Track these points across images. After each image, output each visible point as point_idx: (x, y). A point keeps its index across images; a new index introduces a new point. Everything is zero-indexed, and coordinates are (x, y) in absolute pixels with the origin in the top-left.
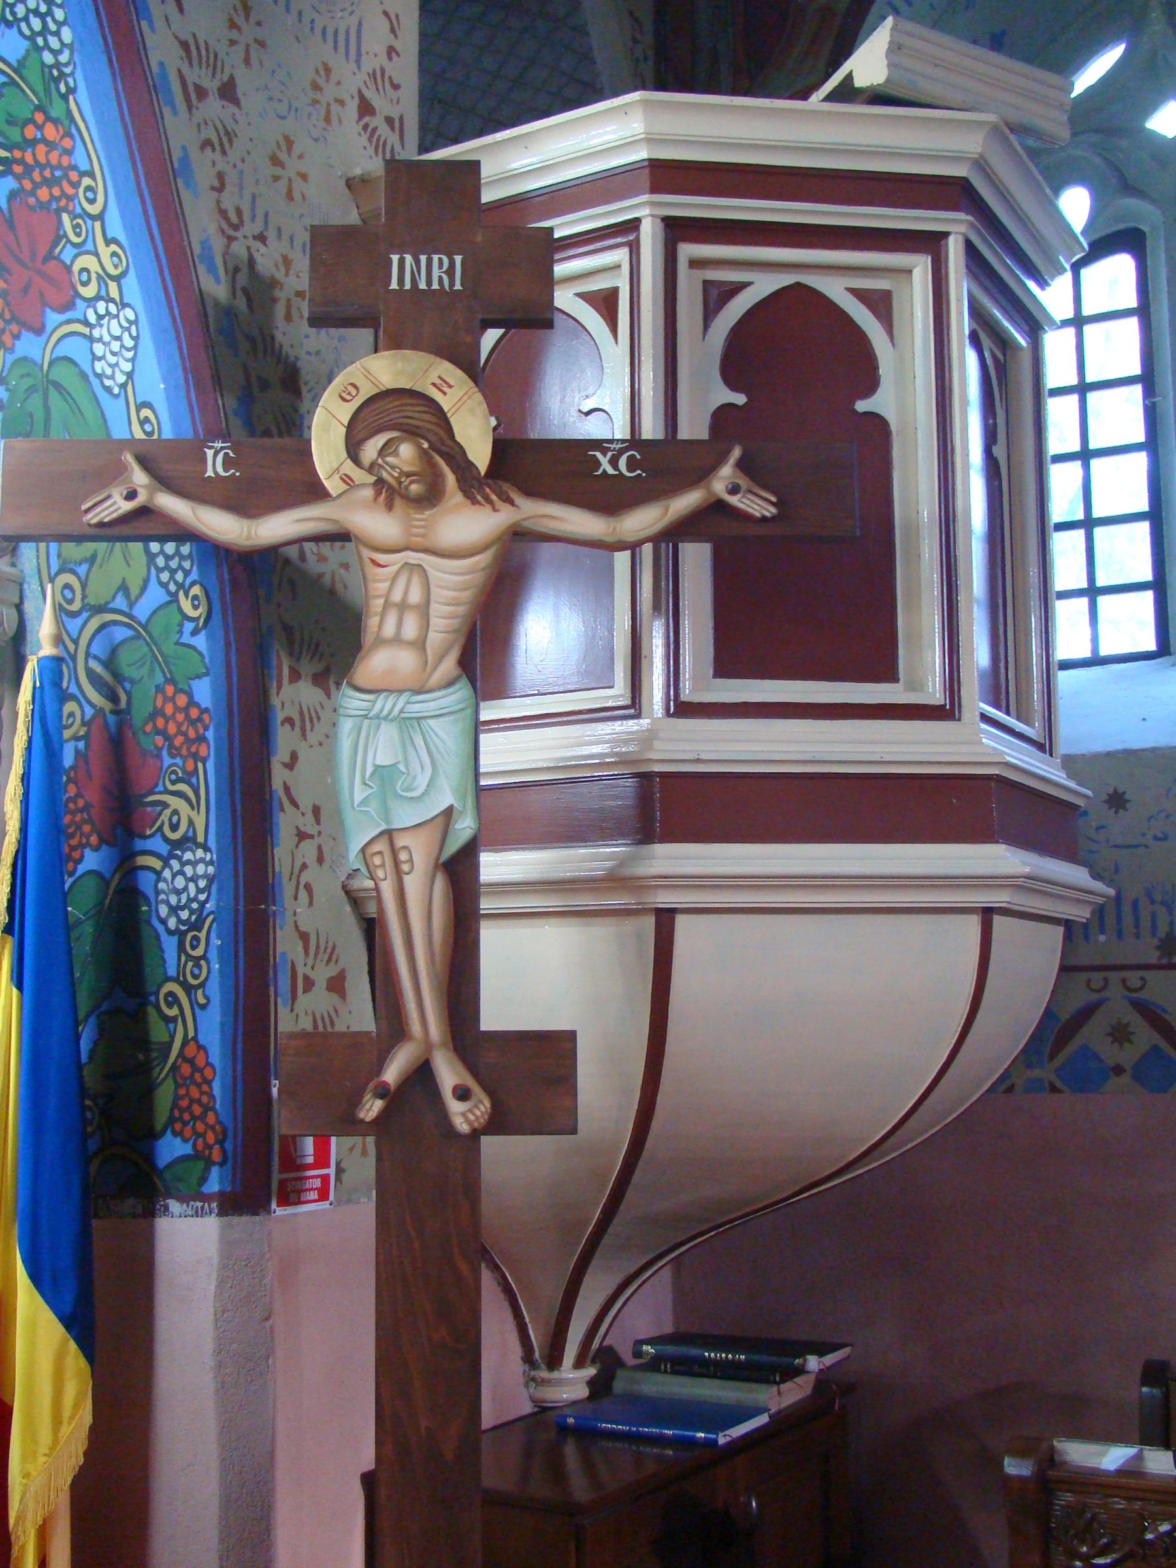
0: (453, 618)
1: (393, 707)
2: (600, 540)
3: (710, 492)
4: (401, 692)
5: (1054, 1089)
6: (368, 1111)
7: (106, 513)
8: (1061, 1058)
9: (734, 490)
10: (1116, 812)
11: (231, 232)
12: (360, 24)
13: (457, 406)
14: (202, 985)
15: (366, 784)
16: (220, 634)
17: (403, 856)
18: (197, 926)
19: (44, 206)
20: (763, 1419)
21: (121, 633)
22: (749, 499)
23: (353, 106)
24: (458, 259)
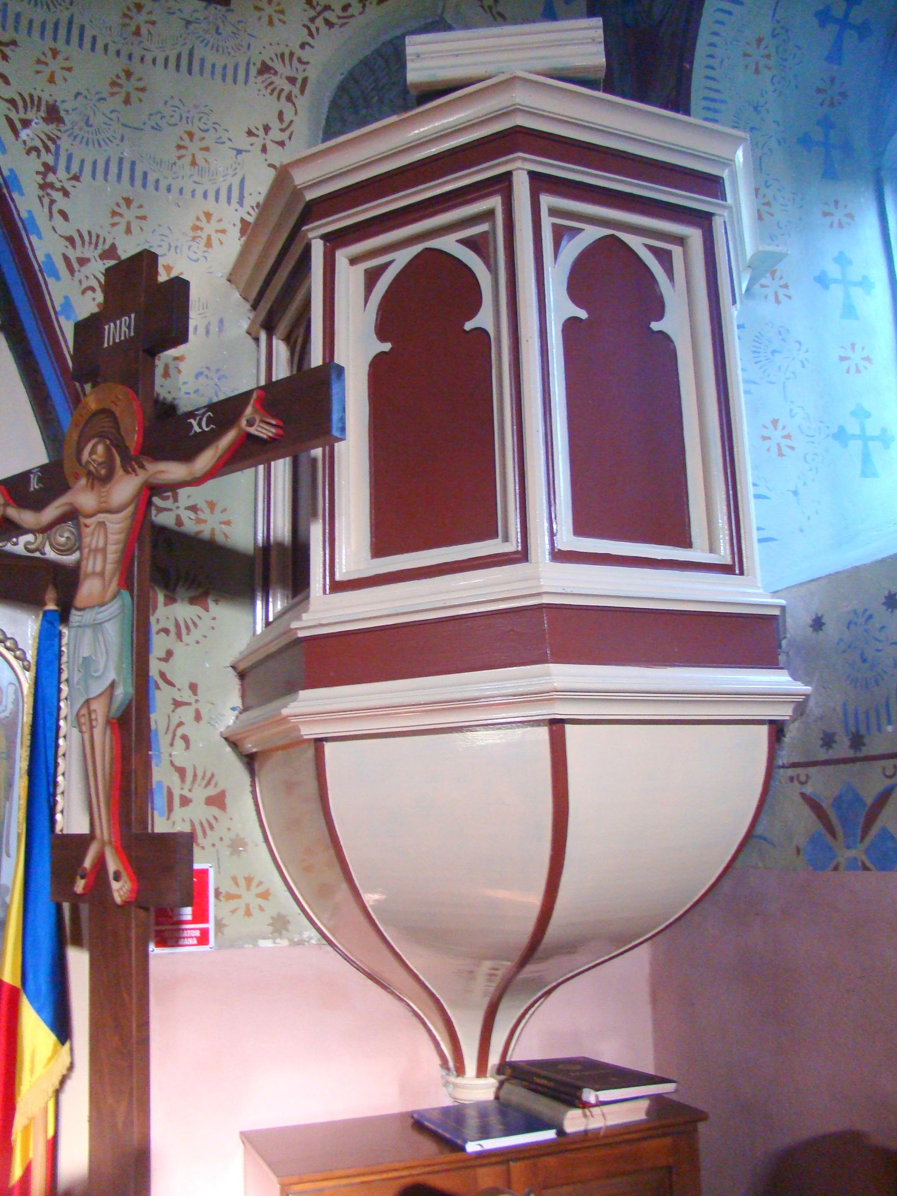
5: (865, 868)
8: (868, 839)
10: (892, 612)
12: (242, 181)
17: (93, 716)
24: (133, 316)
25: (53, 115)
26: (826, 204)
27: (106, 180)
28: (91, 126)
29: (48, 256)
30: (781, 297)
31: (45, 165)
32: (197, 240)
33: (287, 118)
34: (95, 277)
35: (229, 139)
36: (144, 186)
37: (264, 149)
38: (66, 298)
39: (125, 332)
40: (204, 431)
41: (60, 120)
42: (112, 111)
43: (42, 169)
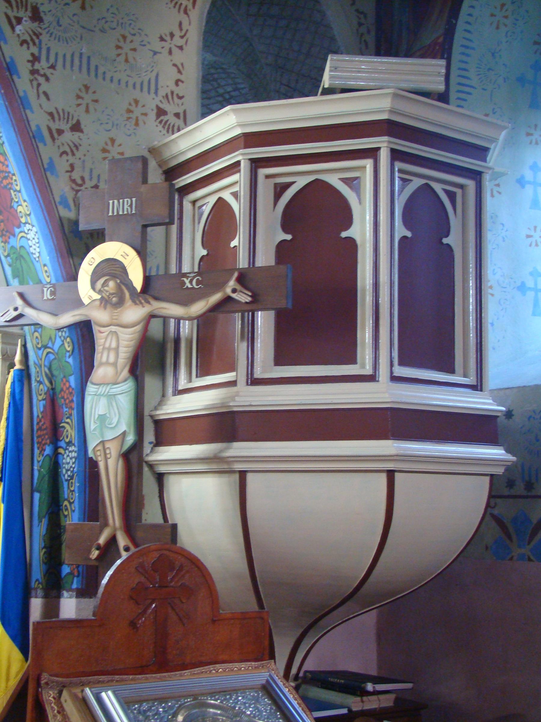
0: (127, 353)
1: (102, 390)
2: (182, 317)
3: (225, 293)
4: (108, 384)
5: (530, 560)
6: (93, 555)
7: (7, 317)
8: (533, 543)
9: (234, 291)
11: (78, 188)
13: (130, 264)
14: (73, 502)
15: (95, 422)
16: (78, 357)
17: (108, 452)
18: (72, 477)
19: (5, 187)
20: (345, 711)
21: (52, 357)
22: (241, 295)
23: (152, 115)
24: (134, 199)
25: (36, 16)
26: (529, 127)
27: (72, 70)
28: (60, 26)
29: (38, 126)
30: (495, 193)
31: (33, 55)
32: (130, 120)
33: (185, 28)
34: (68, 145)
35: (149, 43)
36: (96, 75)
37: (170, 52)
38: (51, 159)
39: (127, 209)
40: (193, 288)
41: (41, 20)
42: (74, 15)
43: (31, 58)
